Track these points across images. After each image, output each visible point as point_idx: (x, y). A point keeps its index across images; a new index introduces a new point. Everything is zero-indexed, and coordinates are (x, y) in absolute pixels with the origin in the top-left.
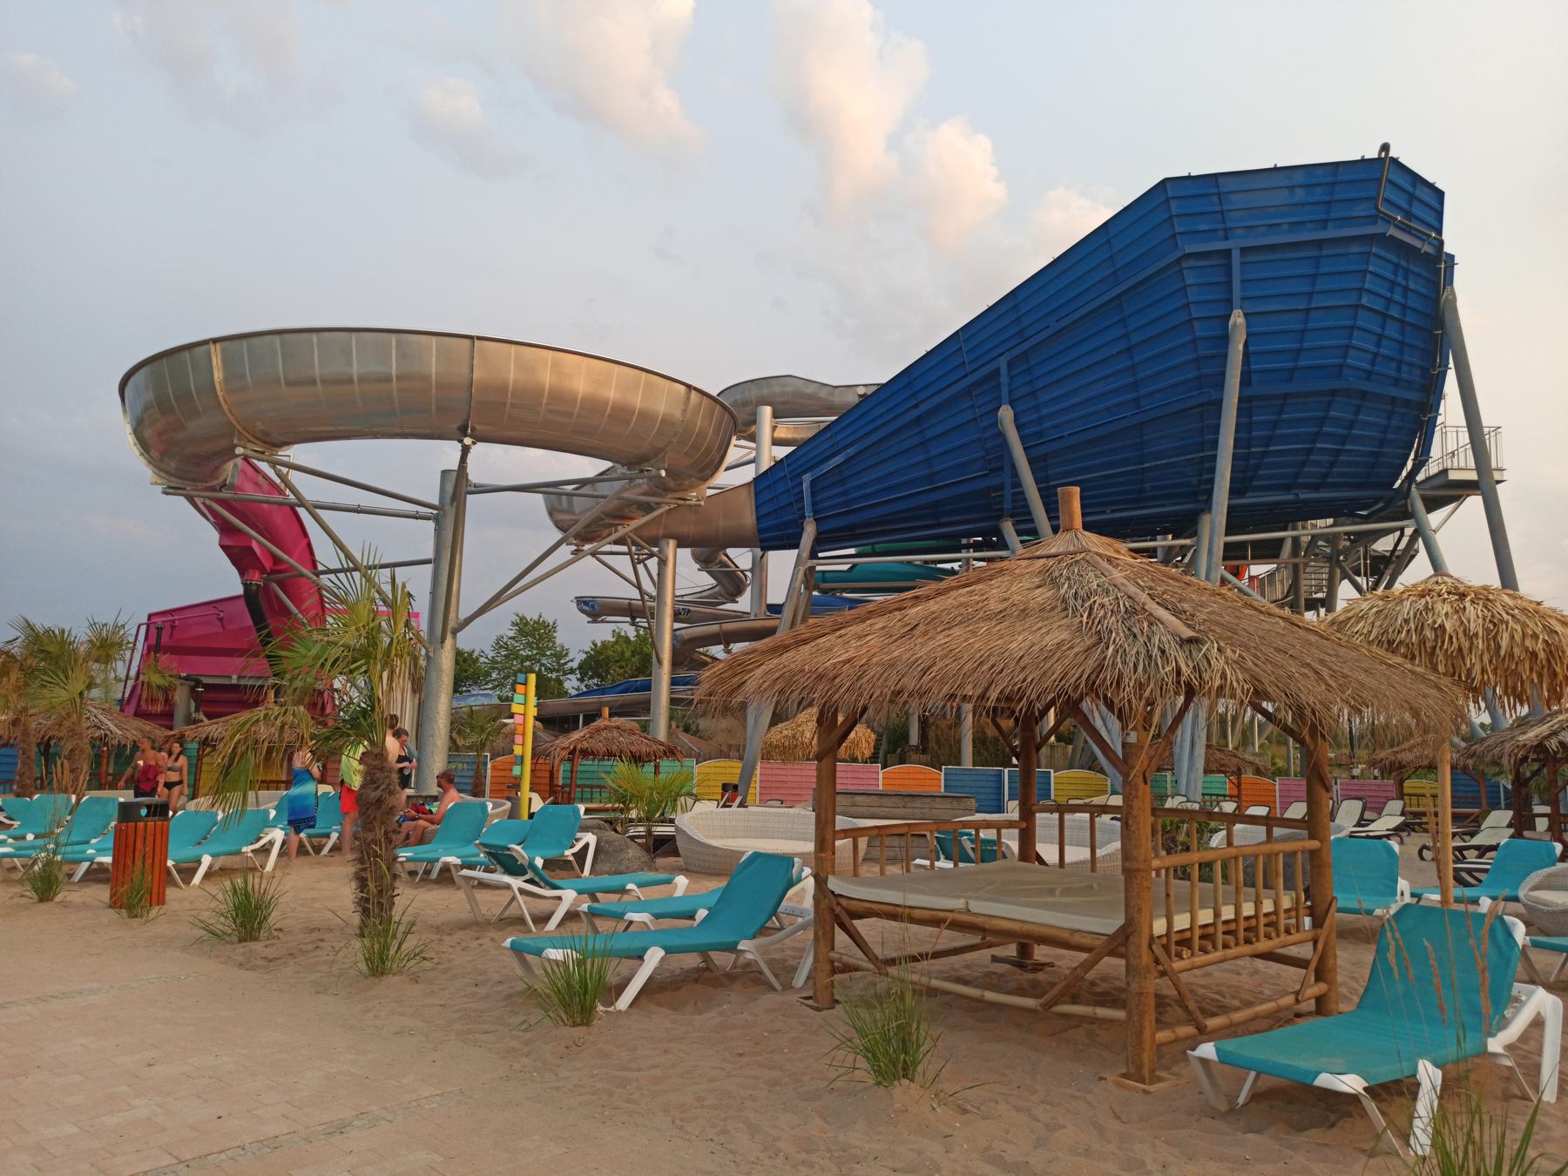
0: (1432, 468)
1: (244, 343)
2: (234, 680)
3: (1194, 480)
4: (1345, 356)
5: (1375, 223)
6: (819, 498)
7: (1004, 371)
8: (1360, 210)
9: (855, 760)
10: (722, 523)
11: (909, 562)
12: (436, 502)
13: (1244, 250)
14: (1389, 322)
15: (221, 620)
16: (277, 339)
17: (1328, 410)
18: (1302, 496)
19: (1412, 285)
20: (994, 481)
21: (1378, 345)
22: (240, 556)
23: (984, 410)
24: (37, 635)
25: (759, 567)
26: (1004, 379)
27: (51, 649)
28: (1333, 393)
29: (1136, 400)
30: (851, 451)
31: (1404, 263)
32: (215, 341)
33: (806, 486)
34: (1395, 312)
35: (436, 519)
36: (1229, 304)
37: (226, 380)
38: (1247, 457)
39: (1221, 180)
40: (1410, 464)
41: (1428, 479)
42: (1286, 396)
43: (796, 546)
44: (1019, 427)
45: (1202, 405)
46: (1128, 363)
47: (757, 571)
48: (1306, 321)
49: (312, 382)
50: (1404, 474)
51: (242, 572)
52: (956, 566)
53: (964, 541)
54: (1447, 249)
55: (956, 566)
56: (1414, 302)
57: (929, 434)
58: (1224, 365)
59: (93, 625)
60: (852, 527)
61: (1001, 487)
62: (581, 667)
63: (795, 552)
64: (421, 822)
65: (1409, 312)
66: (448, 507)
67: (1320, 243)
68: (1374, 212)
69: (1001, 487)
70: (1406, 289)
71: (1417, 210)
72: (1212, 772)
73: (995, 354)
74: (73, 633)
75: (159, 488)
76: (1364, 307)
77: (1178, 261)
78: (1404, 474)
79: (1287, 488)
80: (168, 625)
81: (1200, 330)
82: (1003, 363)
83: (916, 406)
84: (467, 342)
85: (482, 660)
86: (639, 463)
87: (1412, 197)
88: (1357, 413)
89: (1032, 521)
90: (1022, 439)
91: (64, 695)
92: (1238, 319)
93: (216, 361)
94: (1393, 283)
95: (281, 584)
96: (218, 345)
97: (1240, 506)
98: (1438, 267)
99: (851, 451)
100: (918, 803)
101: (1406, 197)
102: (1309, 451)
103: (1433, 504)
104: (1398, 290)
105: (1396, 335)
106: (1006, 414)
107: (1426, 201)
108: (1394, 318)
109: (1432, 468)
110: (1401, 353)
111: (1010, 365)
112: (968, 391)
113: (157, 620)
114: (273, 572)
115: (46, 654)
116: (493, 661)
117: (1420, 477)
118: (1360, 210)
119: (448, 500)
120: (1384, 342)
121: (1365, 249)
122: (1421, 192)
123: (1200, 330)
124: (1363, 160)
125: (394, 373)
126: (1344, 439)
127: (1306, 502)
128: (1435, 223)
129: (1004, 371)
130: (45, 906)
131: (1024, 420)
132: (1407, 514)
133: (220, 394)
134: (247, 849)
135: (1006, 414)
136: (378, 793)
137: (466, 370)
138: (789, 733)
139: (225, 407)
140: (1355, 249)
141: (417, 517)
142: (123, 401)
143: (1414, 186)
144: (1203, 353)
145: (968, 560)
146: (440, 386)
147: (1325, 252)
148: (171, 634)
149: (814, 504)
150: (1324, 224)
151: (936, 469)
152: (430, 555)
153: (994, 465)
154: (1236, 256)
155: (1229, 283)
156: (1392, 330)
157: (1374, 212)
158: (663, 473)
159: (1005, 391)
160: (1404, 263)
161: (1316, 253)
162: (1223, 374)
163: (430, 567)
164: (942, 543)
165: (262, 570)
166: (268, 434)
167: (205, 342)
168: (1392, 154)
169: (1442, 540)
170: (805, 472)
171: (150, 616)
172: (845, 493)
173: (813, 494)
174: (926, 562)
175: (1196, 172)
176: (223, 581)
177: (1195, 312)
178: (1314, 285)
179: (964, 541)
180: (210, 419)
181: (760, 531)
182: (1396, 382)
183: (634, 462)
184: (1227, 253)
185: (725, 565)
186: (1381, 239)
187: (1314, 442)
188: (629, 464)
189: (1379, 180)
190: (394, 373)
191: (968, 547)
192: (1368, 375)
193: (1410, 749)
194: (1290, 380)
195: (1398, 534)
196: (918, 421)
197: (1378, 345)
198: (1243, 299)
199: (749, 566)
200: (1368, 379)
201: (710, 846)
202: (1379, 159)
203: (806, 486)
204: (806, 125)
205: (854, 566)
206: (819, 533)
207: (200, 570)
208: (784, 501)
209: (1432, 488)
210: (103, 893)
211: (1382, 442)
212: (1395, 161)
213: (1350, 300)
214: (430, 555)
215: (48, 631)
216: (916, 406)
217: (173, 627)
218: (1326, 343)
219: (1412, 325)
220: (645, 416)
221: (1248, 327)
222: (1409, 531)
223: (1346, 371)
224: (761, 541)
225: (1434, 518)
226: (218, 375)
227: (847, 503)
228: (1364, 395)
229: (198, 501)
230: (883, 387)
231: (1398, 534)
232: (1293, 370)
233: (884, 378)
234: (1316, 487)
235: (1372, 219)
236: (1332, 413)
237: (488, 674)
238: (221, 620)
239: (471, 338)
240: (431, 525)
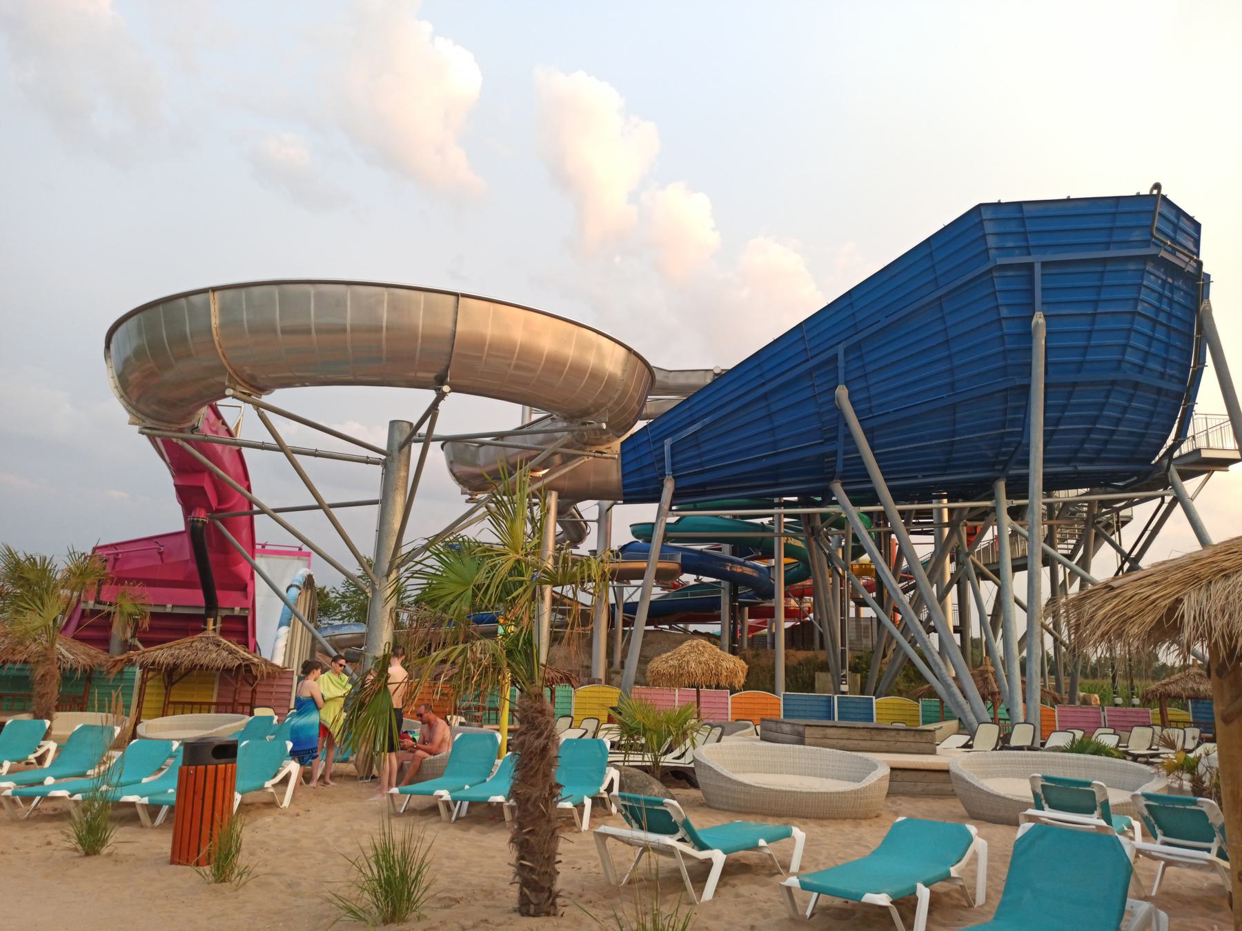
0: (1186, 448)
1: (243, 292)
2: (169, 609)
3: (989, 453)
4: (1123, 353)
5: (1148, 246)
6: (678, 458)
7: (841, 357)
8: (1136, 236)
9: (718, 687)
10: (593, 479)
11: (717, 516)
12: (384, 447)
13: (1044, 264)
14: (1158, 327)
15: (161, 554)
16: (275, 289)
17: (1107, 397)
18: (1080, 468)
19: (1176, 298)
20: (827, 449)
21: (1149, 345)
22: (188, 497)
23: (825, 388)
24: (18, 562)
25: (604, 519)
26: (841, 364)
27: (31, 576)
28: (1113, 383)
29: (952, 384)
30: (707, 420)
31: (1170, 280)
32: (214, 289)
33: (667, 448)
34: (1162, 318)
35: (385, 464)
36: (1031, 308)
37: (222, 326)
38: (1053, 432)
39: (1025, 207)
40: (1169, 442)
41: (1181, 457)
42: (1075, 384)
43: (657, 499)
44: (853, 403)
45: (1006, 390)
46: (946, 354)
47: (603, 521)
48: (1093, 323)
49: (308, 331)
50: (1163, 451)
51: (188, 509)
52: (766, 521)
53: (776, 500)
54: (1205, 269)
55: (766, 521)
56: (1177, 312)
57: (774, 408)
58: (1031, 357)
59: (72, 554)
60: (703, 485)
61: (835, 453)
62: (416, 602)
63: (656, 505)
64: (419, 752)
65: (1173, 320)
66: (396, 454)
67: (1104, 261)
68: (1148, 237)
69: (835, 453)
70: (1171, 301)
71: (1181, 238)
72: (774, 686)
73: (836, 341)
74: (55, 562)
75: (137, 428)
76: (1140, 314)
77: (990, 271)
78: (1163, 451)
79: (1067, 461)
80: (111, 558)
81: (1007, 327)
82: (840, 349)
83: (763, 384)
84: (452, 299)
85: (332, 595)
86: (581, 417)
87: (1176, 228)
88: (1130, 401)
89: (870, 482)
90: (856, 412)
91: (38, 621)
92: (1039, 319)
93: (214, 309)
94: (1161, 295)
95: (223, 521)
96: (217, 294)
97: (1055, 474)
98: (1197, 283)
99: (707, 420)
100: (884, 736)
101: (1171, 226)
102: (1089, 431)
103: (1186, 476)
104: (1165, 300)
105: (1163, 338)
106: (842, 392)
107: (1186, 229)
108: (1162, 324)
109: (1186, 448)
110: (1167, 352)
111: (846, 352)
112: (809, 373)
113: (99, 553)
114: (218, 511)
115: (28, 578)
116: (344, 596)
117: (1176, 454)
118: (1136, 236)
119: (396, 447)
120: (1154, 343)
121: (1141, 267)
122: (1184, 223)
123: (1007, 327)
124: (1138, 196)
125: (384, 324)
126: (1118, 422)
127: (1080, 473)
128: (1195, 250)
129: (841, 357)
130: (93, 861)
131: (855, 398)
132: (1165, 483)
133: (216, 338)
134: (268, 784)
135: (842, 392)
136: (542, 741)
137: (449, 325)
138: (675, 663)
139: (220, 351)
140: (1132, 266)
141: (367, 461)
142: (108, 347)
143: (1178, 219)
144: (1009, 346)
145: (779, 515)
146: (426, 338)
147: (1109, 268)
148: (118, 564)
149: (673, 464)
150: (1107, 245)
151: (779, 437)
152: (377, 496)
153: (828, 436)
154: (1038, 268)
155: (1031, 291)
156: (1160, 334)
157: (1148, 237)
158: (604, 426)
159: (841, 373)
160: (1170, 280)
161: (1100, 269)
162: (1030, 364)
163: (376, 508)
164: (745, 501)
165: (209, 509)
166: (253, 377)
167: (205, 291)
168: (1163, 192)
169: (1198, 505)
170: (666, 437)
171: (95, 549)
172: (700, 455)
173: (672, 456)
174: (735, 516)
175: (1005, 199)
176: (169, 517)
177: (1004, 312)
178: (1099, 294)
179: (776, 500)
180: (182, 365)
181: (624, 486)
182: (1162, 375)
183: (576, 415)
184: (1030, 266)
185: (574, 516)
186: (1154, 259)
187: (1095, 423)
188: (570, 417)
189: (1153, 212)
190: (384, 324)
191: (779, 505)
192: (1141, 369)
193: (1176, 682)
194: (1079, 371)
195: (1159, 500)
196: (765, 397)
197: (1149, 345)
198: (1043, 303)
199: (596, 517)
200: (1140, 373)
201: (741, 784)
202: (1151, 195)
203: (667, 448)
204: (565, 180)
205: (682, 518)
206: (676, 489)
207: (151, 506)
208: (648, 460)
209: (1185, 465)
210: (163, 842)
211: (1147, 425)
212: (1164, 198)
213: (1128, 308)
214: (377, 496)
215: (31, 560)
216: (763, 384)
217: (116, 560)
218: (1109, 342)
219: (1176, 330)
220: (595, 376)
221: (1047, 326)
222: (1168, 499)
223: (1124, 365)
224: (625, 494)
225: (1190, 486)
226: (215, 321)
227: (701, 464)
228: (1136, 385)
229: (159, 440)
230: (729, 372)
231: (1159, 500)
232: (1081, 363)
233: (729, 362)
234: (1090, 461)
235: (1147, 243)
236: (1111, 400)
237: (338, 606)
238: (161, 554)
239: (456, 295)
240: (379, 469)
